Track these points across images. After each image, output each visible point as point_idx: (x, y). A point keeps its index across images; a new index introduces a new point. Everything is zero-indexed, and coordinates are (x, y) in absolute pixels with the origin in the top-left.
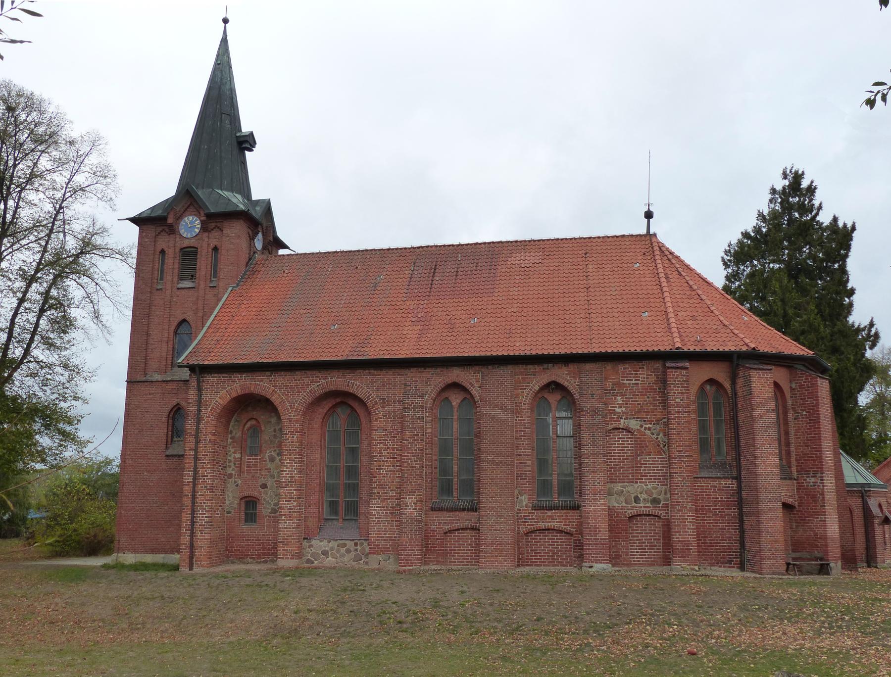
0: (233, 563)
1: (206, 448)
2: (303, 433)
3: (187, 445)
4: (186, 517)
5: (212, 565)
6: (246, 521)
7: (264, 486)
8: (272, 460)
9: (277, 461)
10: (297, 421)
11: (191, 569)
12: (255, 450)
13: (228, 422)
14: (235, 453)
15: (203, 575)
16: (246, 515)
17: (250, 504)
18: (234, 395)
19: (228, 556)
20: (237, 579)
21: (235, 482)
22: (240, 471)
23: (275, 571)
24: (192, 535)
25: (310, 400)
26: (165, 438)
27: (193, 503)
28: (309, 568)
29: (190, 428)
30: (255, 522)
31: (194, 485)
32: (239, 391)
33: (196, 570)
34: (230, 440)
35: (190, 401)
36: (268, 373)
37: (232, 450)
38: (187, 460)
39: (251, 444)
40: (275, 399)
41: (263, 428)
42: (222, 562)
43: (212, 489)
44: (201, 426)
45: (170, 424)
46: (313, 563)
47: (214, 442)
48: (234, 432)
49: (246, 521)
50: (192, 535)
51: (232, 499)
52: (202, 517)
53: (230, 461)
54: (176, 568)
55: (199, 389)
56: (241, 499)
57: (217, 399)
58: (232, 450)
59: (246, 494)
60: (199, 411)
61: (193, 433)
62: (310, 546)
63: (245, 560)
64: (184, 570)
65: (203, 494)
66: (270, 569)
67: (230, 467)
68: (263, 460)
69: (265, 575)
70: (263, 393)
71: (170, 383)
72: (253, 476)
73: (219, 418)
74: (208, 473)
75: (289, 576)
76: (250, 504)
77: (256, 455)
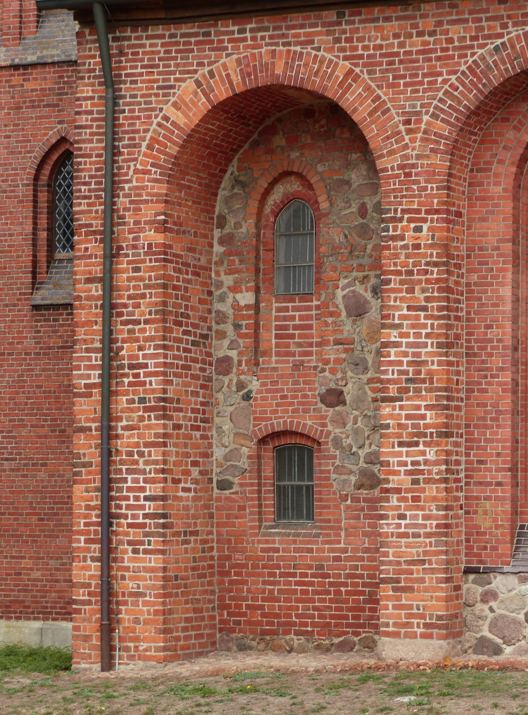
0: (243, 648)
1: (139, 280)
2: (452, 216)
3: (80, 266)
4: (85, 497)
5: (174, 653)
6: (282, 512)
7: (334, 397)
8: (358, 310)
9: (373, 314)
10: (430, 175)
11: (108, 664)
12: (304, 281)
13: (211, 191)
14: (235, 289)
15: (140, 685)
16: (281, 492)
17: (291, 454)
18: (222, 93)
19: (226, 629)
20: (243, 699)
21: (241, 386)
22: (257, 351)
23: (365, 676)
24: (108, 555)
25: (470, 99)
26: (28, 251)
27: (108, 454)
28: (479, 667)
29: (87, 211)
30: (310, 516)
31: (108, 395)
32: (236, 79)
33: (126, 669)
34: (218, 249)
35: (83, 120)
36: (331, 15)
37: (228, 280)
38: (81, 315)
39: (288, 261)
40: (356, 103)
41: (324, 205)
42: (208, 647)
43: (164, 408)
44: (122, 201)
45: (43, 205)
46: (498, 651)
47: (165, 254)
48: (231, 220)
49: (282, 512)
50: (108, 555)
51: (231, 442)
52: (138, 495)
53: (221, 318)
54: (63, 662)
55: (111, 81)
56: (263, 441)
57: (169, 110)
58: (228, 280)
59: (278, 423)
60: (114, 152)
61: (97, 224)
62: (489, 596)
63: (282, 640)
64: (88, 667)
65: (138, 433)
66: (353, 670)
67: (221, 335)
68: (326, 310)
69: (334, 687)
70: (315, 84)
71: (35, 73)
72: (296, 366)
73: (176, 173)
74: (151, 357)
75: (408, 691)
76: (291, 454)
77: (306, 297)
